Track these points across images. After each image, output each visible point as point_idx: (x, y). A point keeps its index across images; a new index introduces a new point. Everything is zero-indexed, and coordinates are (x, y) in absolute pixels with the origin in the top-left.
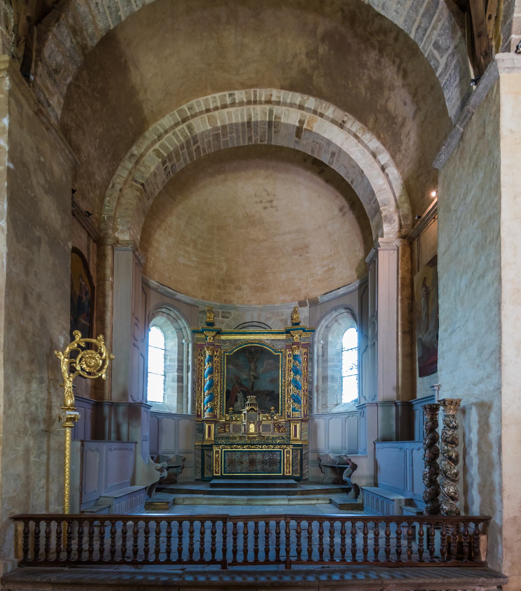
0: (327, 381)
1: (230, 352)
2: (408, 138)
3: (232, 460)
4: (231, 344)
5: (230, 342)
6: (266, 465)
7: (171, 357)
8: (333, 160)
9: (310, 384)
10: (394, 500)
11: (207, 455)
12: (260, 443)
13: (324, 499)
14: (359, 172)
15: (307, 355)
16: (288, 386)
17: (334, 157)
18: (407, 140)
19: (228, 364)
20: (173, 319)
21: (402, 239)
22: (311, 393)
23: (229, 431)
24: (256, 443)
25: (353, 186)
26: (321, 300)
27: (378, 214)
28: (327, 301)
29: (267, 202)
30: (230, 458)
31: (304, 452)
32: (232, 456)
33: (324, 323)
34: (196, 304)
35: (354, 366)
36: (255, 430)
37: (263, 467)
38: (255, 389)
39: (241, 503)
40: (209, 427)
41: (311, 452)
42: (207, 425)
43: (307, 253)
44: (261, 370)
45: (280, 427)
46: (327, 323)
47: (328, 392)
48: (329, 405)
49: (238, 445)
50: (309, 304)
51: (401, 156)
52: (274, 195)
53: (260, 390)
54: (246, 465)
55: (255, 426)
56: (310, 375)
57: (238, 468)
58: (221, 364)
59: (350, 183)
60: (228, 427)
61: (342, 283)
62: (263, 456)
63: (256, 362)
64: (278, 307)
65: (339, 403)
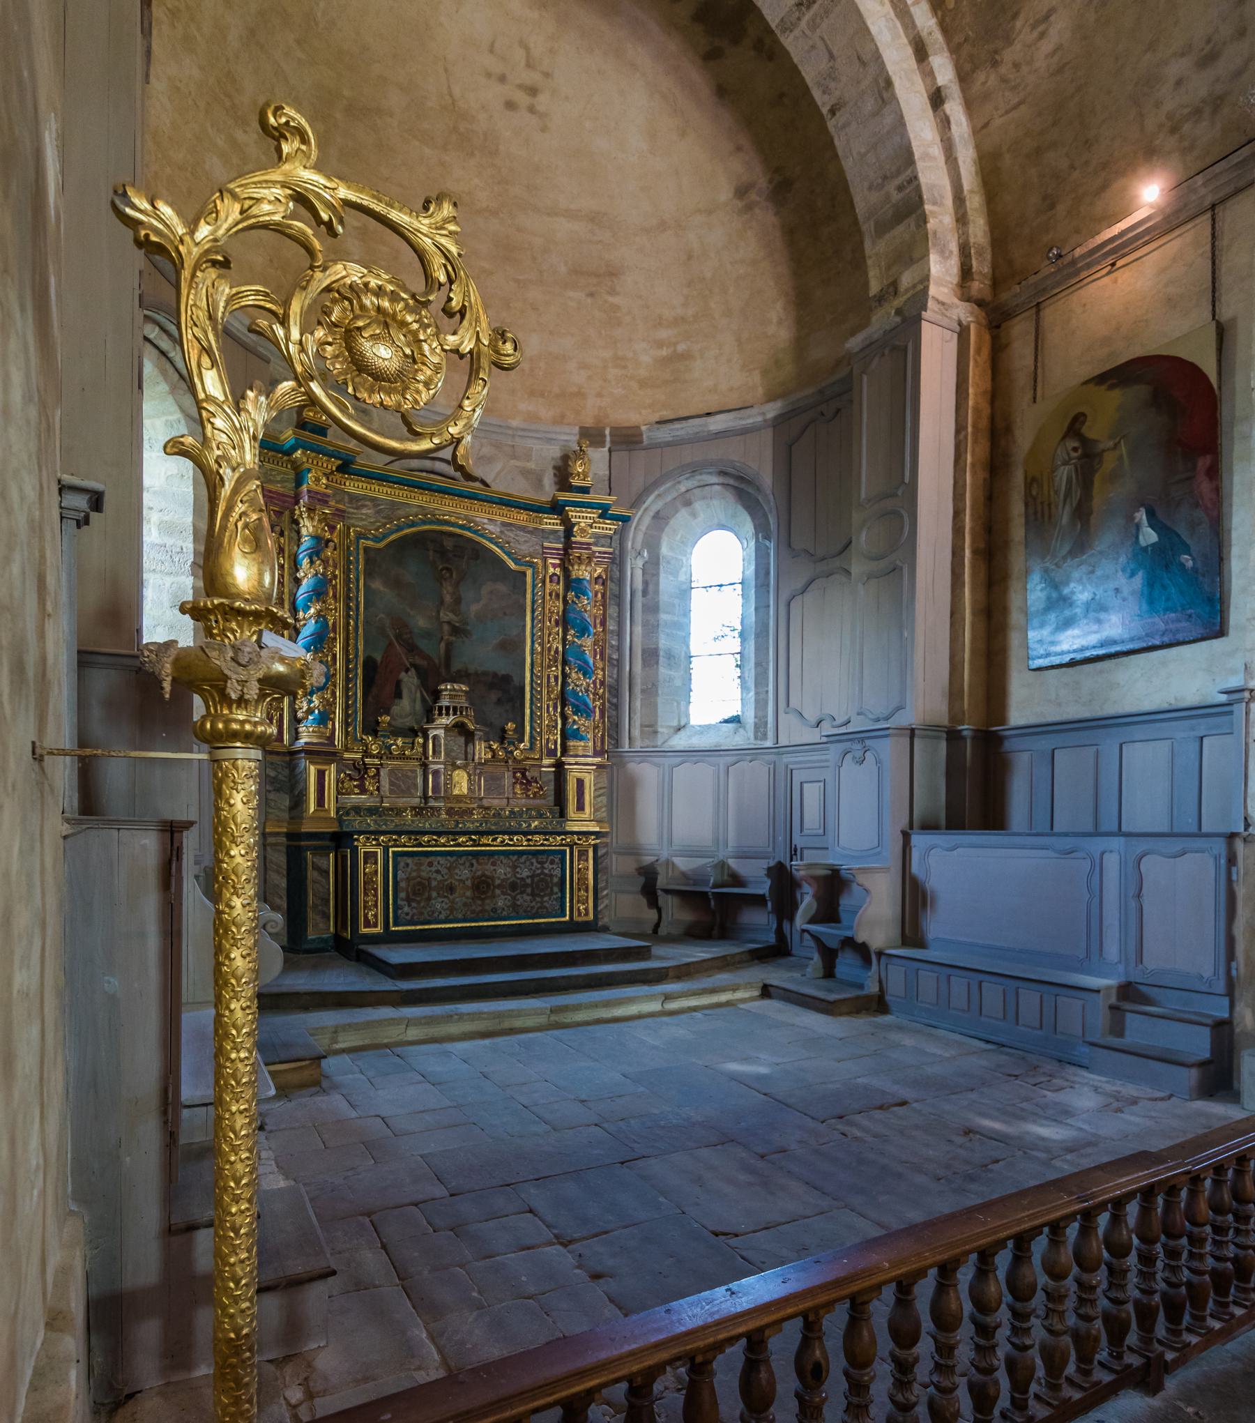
0: (657, 663)
1: (376, 539)
2: (1041, 28)
3: (420, 883)
4: (378, 512)
5: (375, 506)
6: (522, 893)
7: (166, 518)
8: (799, 19)
9: (614, 665)
10: (1098, 991)
11: (316, 867)
12: (484, 827)
13: (749, 985)
14: (876, 80)
15: (603, 584)
16: (550, 667)
17: (808, 8)
18: (1035, 34)
19: (369, 574)
20: (176, 376)
21: (976, 307)
22: (615, 691)
23: (378, 789)
24: (470, 826)
25: (831, 124)
26: (648, 437)
27: (911, 221)
28: (669, 444)
29: (520, 86)
30: (414, 874)
31: (600, 853)
32: (418, 870)
33: (652, 503)
34: (261, 349)
35: (727, 631)
36: (469, 789)
37: (514, 898)
38: (456, 666)
39: (530, 1022)
40: (321, 775)
41: (615, 853)
42: (312, 768)
43: (612, 292)
44: (474, 608)
45: (529, 783)
46: (659, 505)
47: (660, 692)
48: (662, 727)
49: (439, 834)
50: (612, 442)
51: (993, 80)
52: (547, 75)
53: (472, 669)
54: (463, 896)
55: (469, 775)
56: (614, 643)
57: (439, 904)
58: (347, 572)
59: (825, 111)
60: (373, 777)
61: (713, 402)
62: (514, 867)
63: (457, 585)
64: (517, 429)
65: (682, 723)
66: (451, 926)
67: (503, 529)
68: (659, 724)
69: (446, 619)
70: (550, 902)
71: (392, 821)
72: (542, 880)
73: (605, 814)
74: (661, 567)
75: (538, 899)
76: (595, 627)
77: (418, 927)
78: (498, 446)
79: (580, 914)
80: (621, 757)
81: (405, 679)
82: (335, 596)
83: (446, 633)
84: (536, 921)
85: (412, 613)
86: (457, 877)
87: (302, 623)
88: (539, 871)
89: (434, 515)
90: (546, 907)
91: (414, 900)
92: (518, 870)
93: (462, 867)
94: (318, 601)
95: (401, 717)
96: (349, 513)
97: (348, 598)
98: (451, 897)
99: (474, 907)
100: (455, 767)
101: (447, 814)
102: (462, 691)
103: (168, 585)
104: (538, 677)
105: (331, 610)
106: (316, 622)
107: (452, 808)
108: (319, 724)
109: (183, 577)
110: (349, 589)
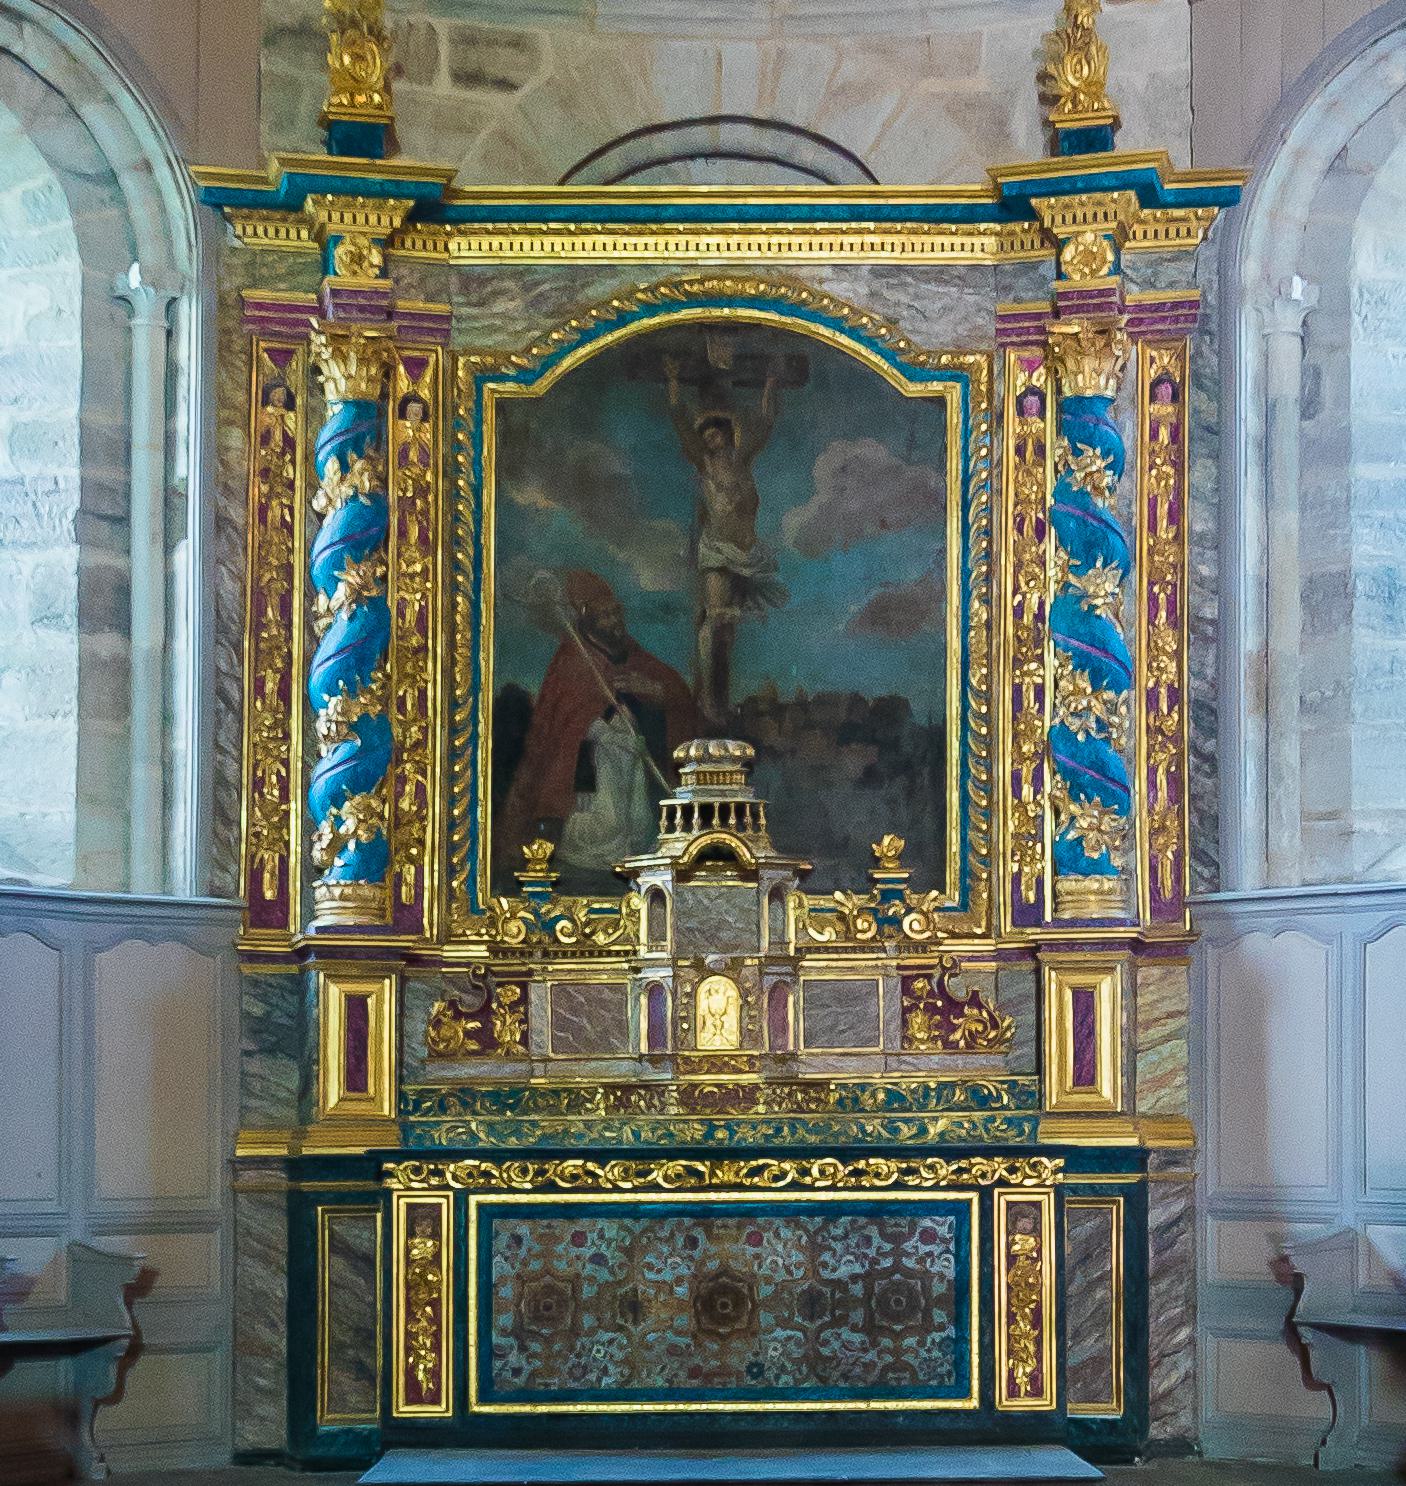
1: (526, 376)
3: (549, 1290)
4: (535, 303)
6: (837, 1322)
7: (26, 416)
9: (1206, 639)
11: (339, 1247)
19: (508, 471)
22: (1209, 715)
24: (749, 1137)
30: (536, 1265)
31: (1156, 1217)
32: (546, 1255)
38: (744, 686)
40: (356, 1008)
41: (1213, 1212)
44: (794, 521)
46: (1336, 135)
47: (1357, 707)
48: (1366, 815)
56: (1205, 570)
58: (452, 471)
60: (513, 1007)
62: (815, 1248)
66: (636, 1407)
67: (877, 285)
68: (1355, 807)
69: (715, 560)
70: (921, 1349)
71: (534, 1124)
72: (897, 1288)
73: (1183, 1095)
74: (1356, 319)
75: (886, 1342)
76: (1153, 528)
77: (542, 1409)
78: (883, 50)
79: (1013, 1392)
80: (1227, 916)
81: (604, 738)
82: (423, 538)
83: (714, 599)
84: (876, 1405)
85: (621, 556)
86: (651, 1276)
87: (323, 623)
88: (887, 1263)
89: (678, 285)
90: (907, 1367)
91: (535, 1335)
92: (826, 1257)
93: (838, 1246)
94: (357, 561)
95: (594, 840)
96: (459, 319)
97: (454, 542)
98: (636, 1330)
99: (697, 1360)
100: (703, 971)
101: (681, 1103)
102: (734, 760)
103: (27, 571)
104: (978, 694)
105: (412, 576)
106: (351, 619)
107: (694, 1086)
108: (356, 877)
109: (58, 549)
110: (457, 517)
